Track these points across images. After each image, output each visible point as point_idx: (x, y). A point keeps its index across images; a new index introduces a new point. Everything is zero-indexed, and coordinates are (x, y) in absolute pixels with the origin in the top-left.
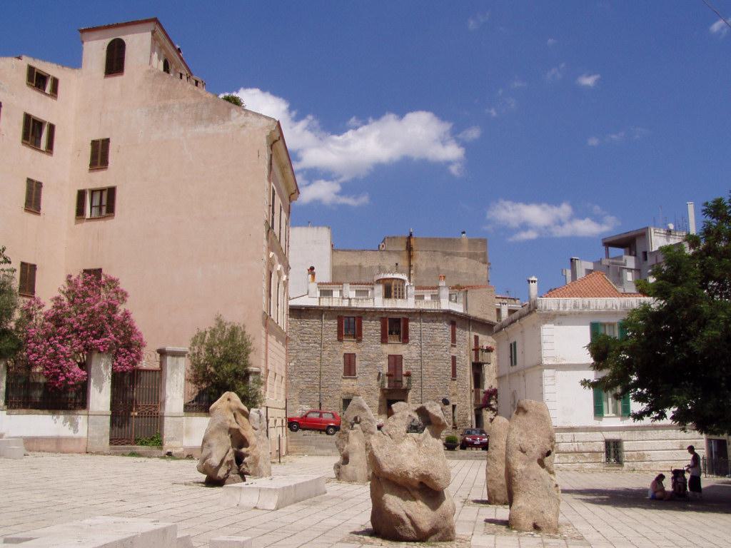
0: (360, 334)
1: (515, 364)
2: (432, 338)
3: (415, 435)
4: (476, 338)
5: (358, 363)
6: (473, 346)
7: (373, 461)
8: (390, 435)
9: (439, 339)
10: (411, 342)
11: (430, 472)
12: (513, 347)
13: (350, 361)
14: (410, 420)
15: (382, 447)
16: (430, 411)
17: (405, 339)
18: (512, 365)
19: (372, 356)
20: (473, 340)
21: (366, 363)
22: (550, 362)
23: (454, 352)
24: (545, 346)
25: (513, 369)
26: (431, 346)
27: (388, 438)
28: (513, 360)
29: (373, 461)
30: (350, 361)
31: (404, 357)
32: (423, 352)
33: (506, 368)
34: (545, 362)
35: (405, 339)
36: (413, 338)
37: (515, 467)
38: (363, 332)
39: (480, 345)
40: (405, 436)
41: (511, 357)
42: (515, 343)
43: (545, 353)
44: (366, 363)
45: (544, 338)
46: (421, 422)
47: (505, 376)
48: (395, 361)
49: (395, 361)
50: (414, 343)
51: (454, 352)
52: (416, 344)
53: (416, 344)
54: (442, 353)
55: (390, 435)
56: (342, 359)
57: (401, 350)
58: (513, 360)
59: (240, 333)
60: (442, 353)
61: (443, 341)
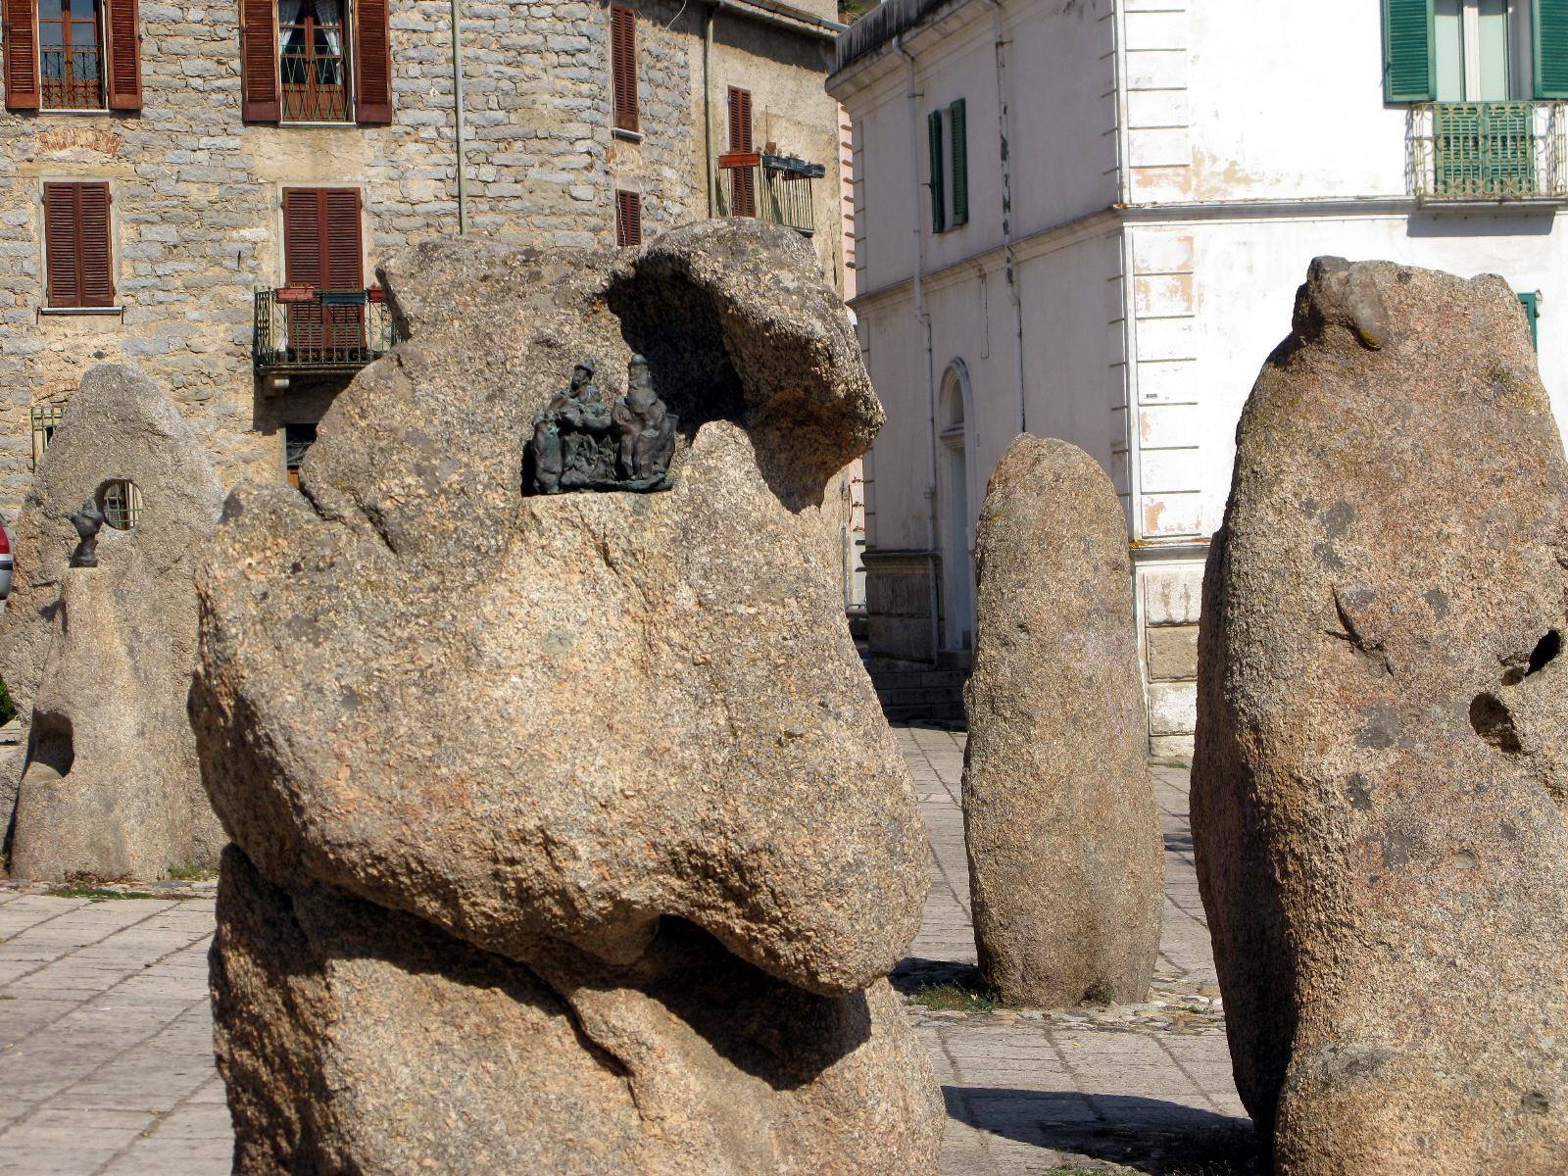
0: (129, 82)
1: (963, 217)
2: (515, 101)
3: (602, 508)
4: (740, 101)
5: (121, 233)
6: (723, 144)
7: (233, 748)
8: (374, 515)
9: (549, 105)
10: (404, 118)
11: (759, 834)
12: (947, 132)
13: (77, 224)
14: (548, 384)
15: (310, 627)
16: (736, 285)
17: (372, 101)
18: (940, 227)
19: (196, 194)
20: (722, 112)
21: (170, 233)
22: (1165, 194)
23: (630, 166)
24: (1135, 109)
25: (953, 245)
26: (507, 141)
27: (359, 549)
28: (948, 202)
29: (233, 748)
30: (77, 224)
31: (368, 198)
32: (468, 172)
33: (912, 242)
34: (1137, 193)
35: (372, 101)
36: (418, 99)
37: (1305, 762)
38: (146, 68)
39: (758, 142)
40: (516, 525)
41: (937, 186)
42: (959, 110)
43: (1137, 148)
44: (170, 233)
45: (1130, 69)
46: (646, 397)
47: (900, 287)
48: (322, 223)
49: (322, 223)
50: (416, 127)
51: (630, 166)
52: (428, 133)
53: (428, 133)
54: (566, 177)
55: (374, 515)
56: (34, 216)
57: (351, 160)
58: (948, 202)
59: (571, 889)
60: (566, 177)
61: (571, 115)
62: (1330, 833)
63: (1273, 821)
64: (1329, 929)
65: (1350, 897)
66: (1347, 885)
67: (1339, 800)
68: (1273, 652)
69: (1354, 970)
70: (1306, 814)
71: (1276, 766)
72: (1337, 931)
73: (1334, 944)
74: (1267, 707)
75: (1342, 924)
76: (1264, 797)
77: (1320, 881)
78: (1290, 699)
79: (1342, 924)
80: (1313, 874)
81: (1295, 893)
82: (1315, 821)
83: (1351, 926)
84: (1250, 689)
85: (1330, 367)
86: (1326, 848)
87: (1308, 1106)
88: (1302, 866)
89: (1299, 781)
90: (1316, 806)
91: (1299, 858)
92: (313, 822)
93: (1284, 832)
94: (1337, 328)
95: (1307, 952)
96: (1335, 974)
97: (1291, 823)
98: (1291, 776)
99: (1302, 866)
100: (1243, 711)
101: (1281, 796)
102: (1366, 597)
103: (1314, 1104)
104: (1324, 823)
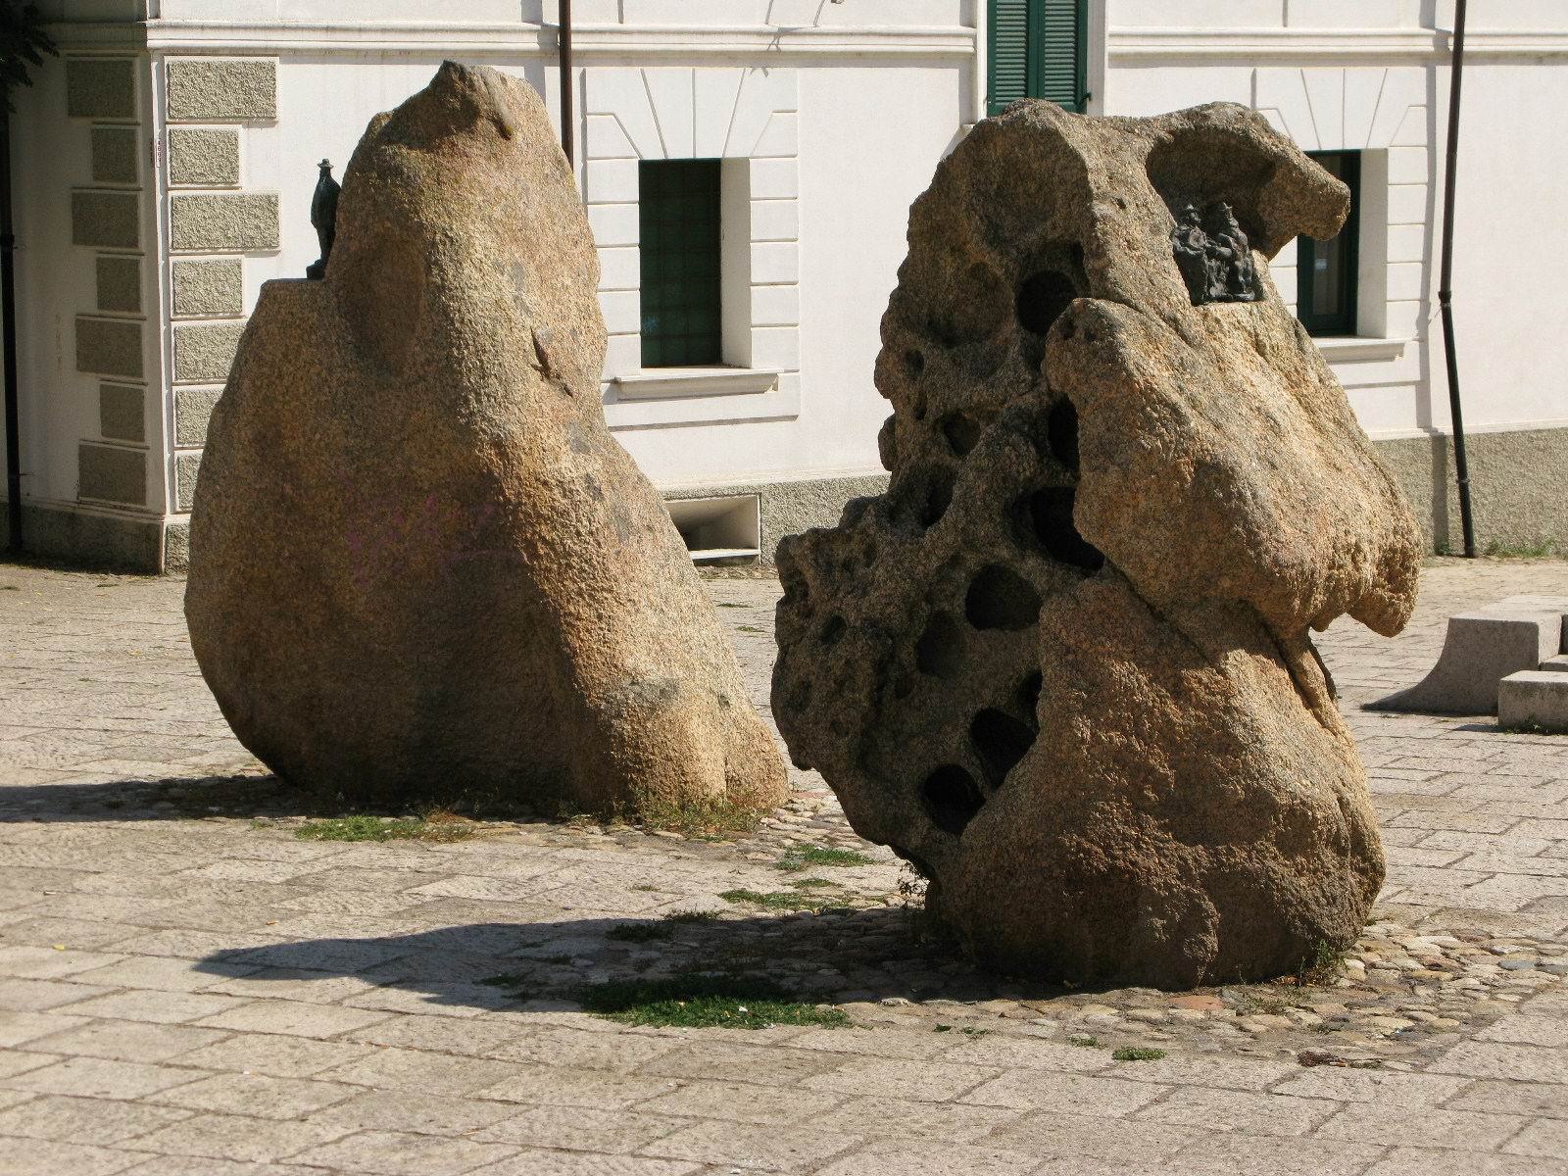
37: (548, 470)
62: (579, 521)
63: (521, 516)
64: (590, 595)
65: (607, 569)
66: (601, 559)
67: (583, 496)
68: (505, 383)
69: (618, 626)
70: (553, 508)
71: (523, 473)
72: (598, 595)
73: (597, 605)
74: (508, 427)
75: (603, 589)
76: (513, 498)
77: (576, 559)
78: (524, 420)
79: (603, 589)
80: (568, 554)
81: (549, 570)
82: (564, 513)
83: (610, 591)
84: (489, 413)
85: (479, 152)
86: (578, 534)
87: (645, 728)
88: (554, 550)
89: (545, 483)
90: (562, 503)
91: (550, 544)
92: (1267, 551)
93: (532, 525)
94: (485, 121)
95: (571, 614)
96: (601, 629)
97: (539, 516)
98: (537, 480)
99: (554, 550)
100: (484, 431)
101: (529, 496)
102: (550, 337)
103: (649, 725)
104: (573, 515)
